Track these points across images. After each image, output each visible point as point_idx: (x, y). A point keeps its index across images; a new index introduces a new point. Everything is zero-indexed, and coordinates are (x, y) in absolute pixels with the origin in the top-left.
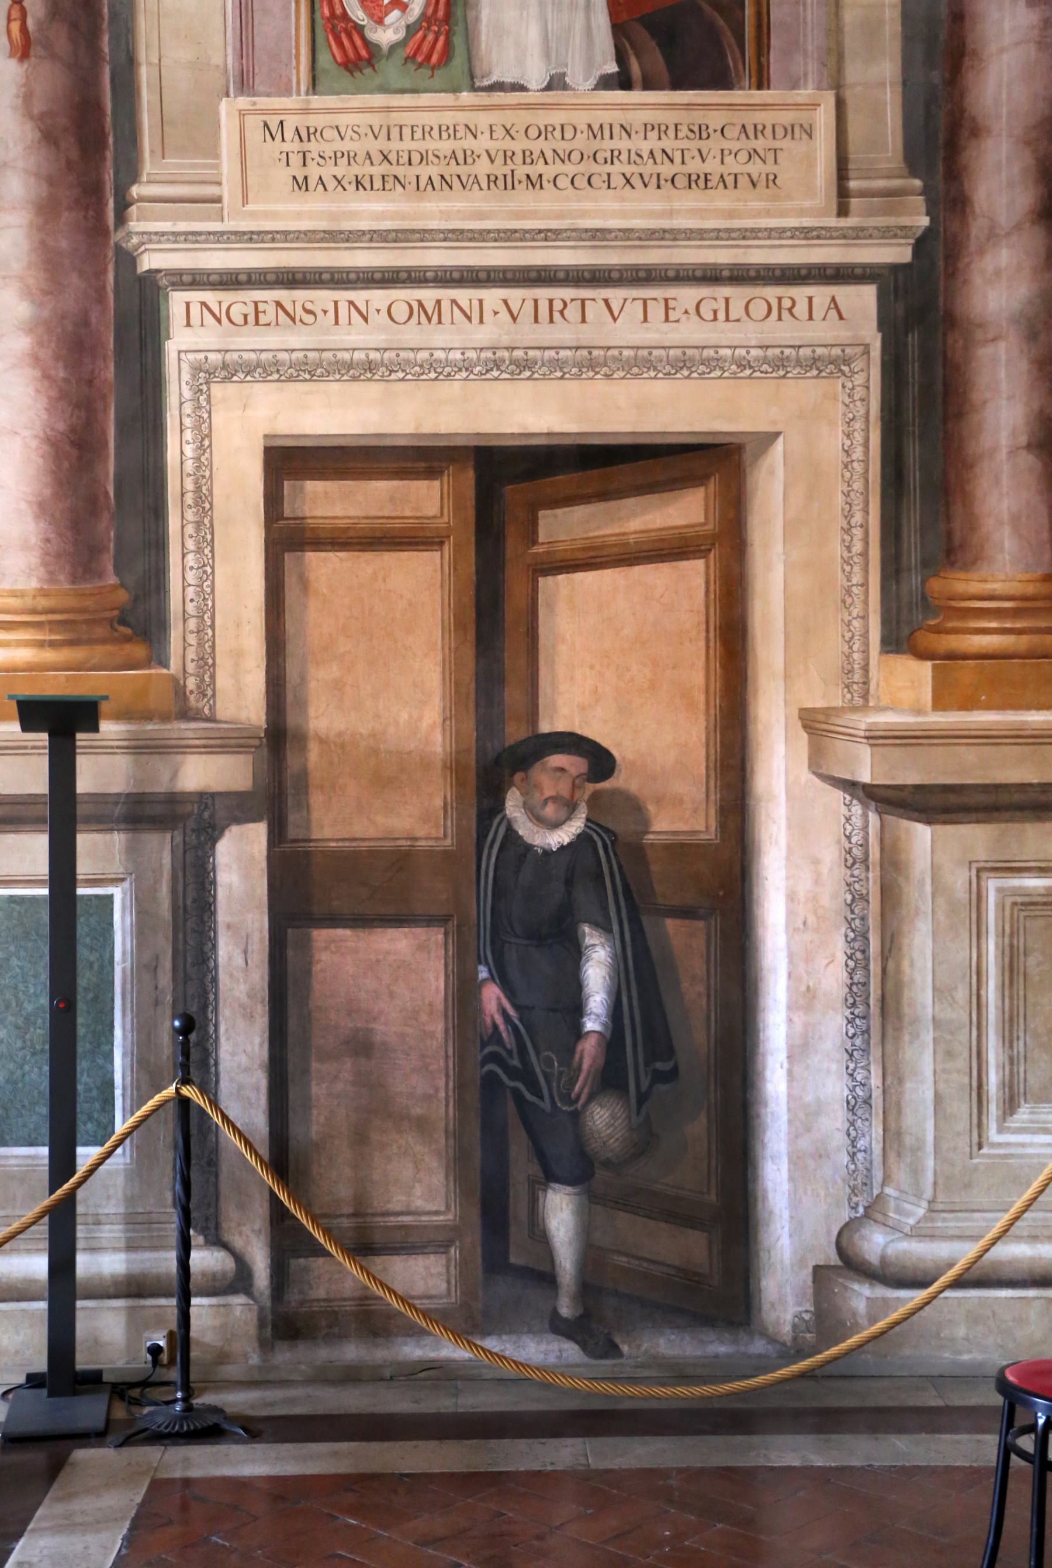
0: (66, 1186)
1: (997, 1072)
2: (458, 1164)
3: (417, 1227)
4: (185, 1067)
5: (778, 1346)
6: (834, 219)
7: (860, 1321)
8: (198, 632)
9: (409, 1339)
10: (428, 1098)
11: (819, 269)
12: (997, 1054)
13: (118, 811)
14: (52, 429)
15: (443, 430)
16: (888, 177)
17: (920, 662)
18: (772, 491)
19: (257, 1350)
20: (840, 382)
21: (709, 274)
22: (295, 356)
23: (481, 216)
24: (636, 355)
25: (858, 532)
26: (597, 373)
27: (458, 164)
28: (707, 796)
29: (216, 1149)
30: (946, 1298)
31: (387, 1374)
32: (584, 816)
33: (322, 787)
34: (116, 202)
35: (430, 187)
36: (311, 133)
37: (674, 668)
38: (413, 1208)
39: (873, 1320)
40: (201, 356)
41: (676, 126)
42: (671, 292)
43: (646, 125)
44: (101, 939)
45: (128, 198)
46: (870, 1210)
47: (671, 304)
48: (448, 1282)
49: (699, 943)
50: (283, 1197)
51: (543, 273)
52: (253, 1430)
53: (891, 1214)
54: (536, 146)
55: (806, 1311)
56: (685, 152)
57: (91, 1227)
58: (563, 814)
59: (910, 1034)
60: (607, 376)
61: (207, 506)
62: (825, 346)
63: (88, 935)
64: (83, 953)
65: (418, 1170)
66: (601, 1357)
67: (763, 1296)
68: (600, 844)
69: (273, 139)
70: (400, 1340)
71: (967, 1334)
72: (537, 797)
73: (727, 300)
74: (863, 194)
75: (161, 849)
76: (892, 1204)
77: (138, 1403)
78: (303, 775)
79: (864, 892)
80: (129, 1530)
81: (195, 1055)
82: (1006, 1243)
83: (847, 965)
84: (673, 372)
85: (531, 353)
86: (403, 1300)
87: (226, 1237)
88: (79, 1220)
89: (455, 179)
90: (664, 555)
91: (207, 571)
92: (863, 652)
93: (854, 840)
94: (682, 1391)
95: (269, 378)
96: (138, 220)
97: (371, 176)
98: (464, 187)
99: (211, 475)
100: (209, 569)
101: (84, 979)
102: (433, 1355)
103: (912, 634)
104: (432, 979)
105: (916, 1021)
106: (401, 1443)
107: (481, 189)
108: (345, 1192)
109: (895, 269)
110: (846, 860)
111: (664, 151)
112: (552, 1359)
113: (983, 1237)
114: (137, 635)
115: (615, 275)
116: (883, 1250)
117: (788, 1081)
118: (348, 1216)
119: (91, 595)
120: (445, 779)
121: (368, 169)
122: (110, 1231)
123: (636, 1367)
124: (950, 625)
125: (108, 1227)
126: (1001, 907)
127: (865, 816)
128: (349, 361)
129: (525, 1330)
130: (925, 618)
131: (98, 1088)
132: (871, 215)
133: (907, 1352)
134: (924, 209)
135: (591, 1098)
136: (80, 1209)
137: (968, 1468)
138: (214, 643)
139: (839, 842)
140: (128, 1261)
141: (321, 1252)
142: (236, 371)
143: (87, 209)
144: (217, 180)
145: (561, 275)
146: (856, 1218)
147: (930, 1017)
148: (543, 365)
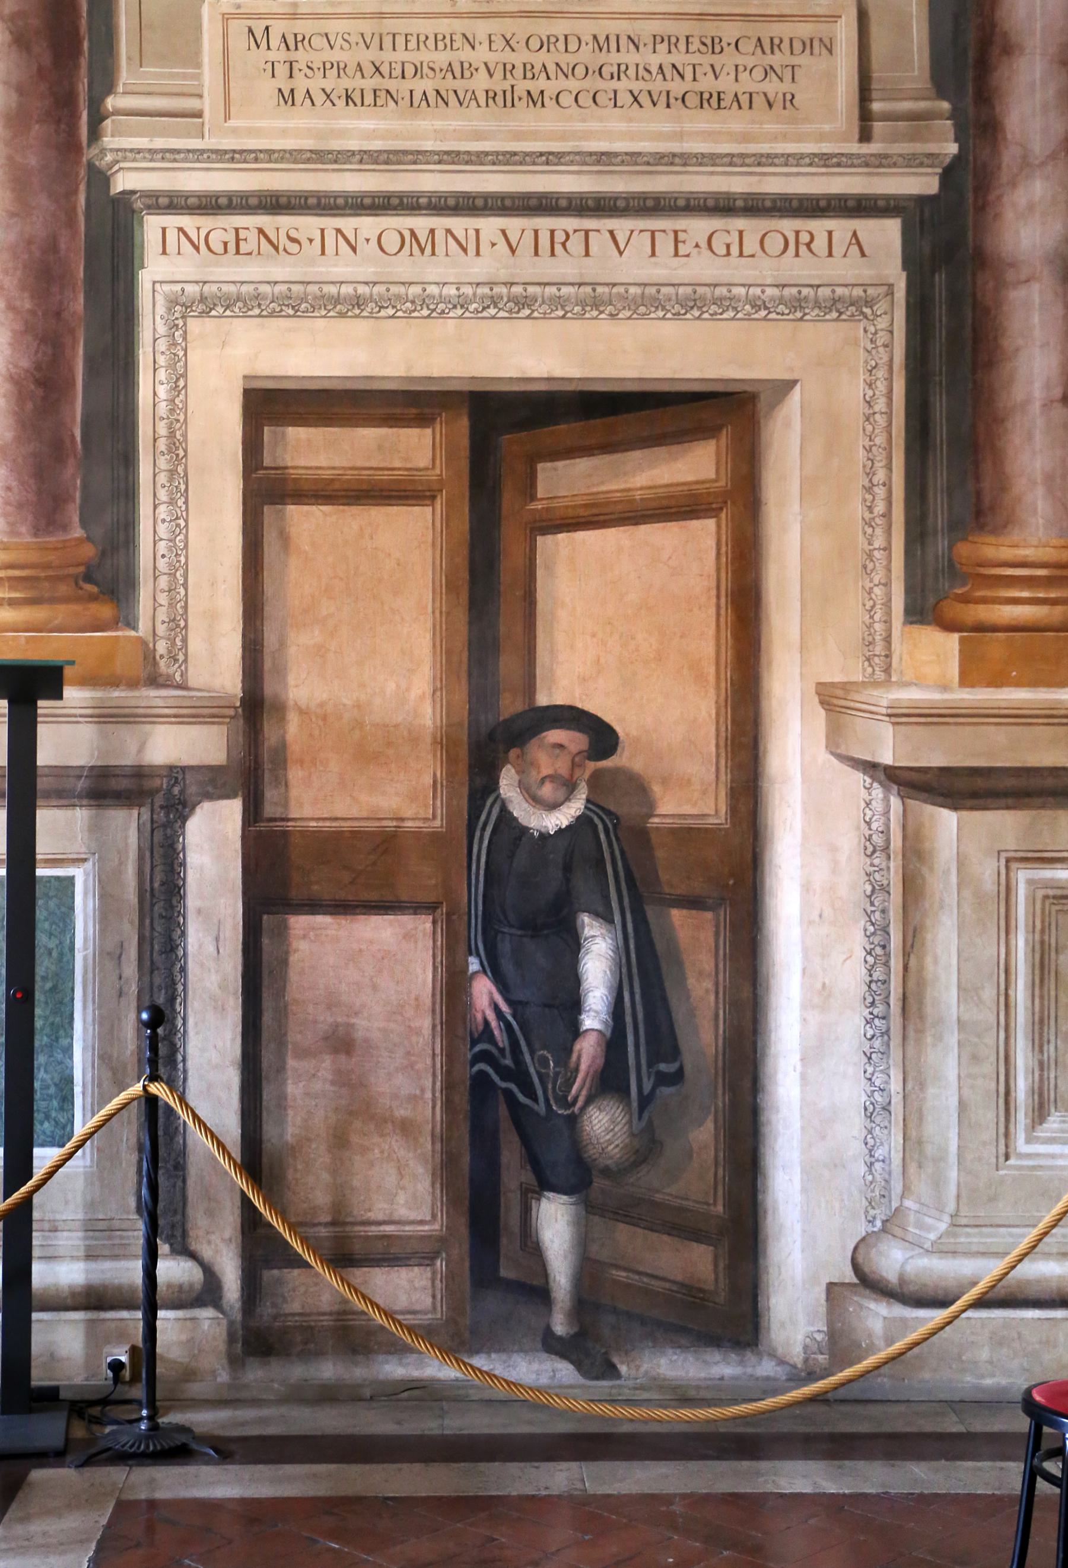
0: (23, 1189)
1: (1026, 1079)
2: (446, 1169)
3: (400, 1237)
4: (153, 1062)
5: (788, 1368)
6: (857, 145)
7: (877, 1342)
8: (170, 591)
9: (390, 1357)
10: (413, 1099)
11: (840, 200)
12: (1026, 1058)
13: (81, 785)
14: (16, 366)
15: (436, 374)
16: (916, 99)
17: (946, 634)
18: (789, 444)
19: (226, 1366)
20: (862, 325)
21: (722, 205)
22: (278, 288)
23: (478, 136)
24: (643, 293)
25: (880, 492)
26: (601, 312)
27: (454, 78)
28: (717, 777)
29: (183, 1152)
30: (969, 1318)
31: (367, 1393)
32: (584, 796)
33: (301, 762)
34: (89, 115)
35: (424, 103)
36: (298, 41)
37: (681, 637)
38: (396, 1217)
39: (889, 1342)
40: (178, 288)
41: (687, 38)
42: (681, 223)
43: (655, 36)
44: (61, 925)
45: (102, 110)
46: (888, 1224)
47: (682, 236)
48: (434, 1297)
49: (707, 936)
50: (259, 1203)
51: (544, 201)
52: (225, 1450)
53: (910, 1229)
54: (538, 59)
55: (819, 1331)
56: (697, 67)
57: (47, 1234)
58: (561, 795)
59: (934, 1036)
60: (612, 316)
61: (181, 453)
62: (846, 286)
63: (46, 919)
64: (42, 939)
65: (401, 1176)
66: (597, 1378)
67: (772, 1315)
68: (600, 827)
69: (258, 47)
70: (381, 1358)
71: (991, 1357)
72: (534, 776)
73: (741, 233)
74: (887, 117)
75: (127, 826)
76: (912, 1218)
77: (99, 1421)
78: (282, 747)
79: (885, 882)
80: (96, 1552)
81: (163, 1050)
82: (1033, 1260)
83: (866, 962)
84: (683, 311)
85: (531, 289)
86: (388, 1314)
87: (194, 1246)
88: (35, 1226)
89: (451, 93)
90: (672, 514)
91: (180, 524)
92: (885, 622)
93: (874, 826)
94: (687, 1413)
95: (250, 313)
96: (112, 136)
97: (362, 90)
98: (461, 104)
99: (186, 419)
100: (182, 523)
101: (43, 966)
102: (416, 1374)
103: (937, 603)
104: (419, 971)
105: (940, 1021)
106: (385, 1465)
107: (479, 106)
108: (322, 1198)
109: (921, 200)
110: (866, 848)
111: (674, 66)
112: (544, 1380)
113: (1009, 1253)
114: (104, 594)
115: (621, 204)
116: (902, 1266)
117: (801, 1086)
118: (326, 1225)
119: (56, 549)
120: (435, 756)
121: (358, 83)
122: (68, 1239)
123: (635, 1389)
124: (979, 594)
125: (65, 1234)
126: (1031, 900)
127: (886, 800)
128: (336, 295)
129: (516, 1348)
130: (952, 587)
131: (56, 1085)
132: (895, 142)
133: (927, 1375)
134: (952, 136)
135: (588, 1101)
136: (36, 1215)
137: (989, 1496)
138: (186, 603)
139: (858, 828)
140: (87, 1271)
141: (300, 1263)
142: (215, 305)
143: (59, 121)
144: (197, 92)
145: (563, 203)
146: (873, 1232)
147: (955, 1018)
148: (543, 302)
